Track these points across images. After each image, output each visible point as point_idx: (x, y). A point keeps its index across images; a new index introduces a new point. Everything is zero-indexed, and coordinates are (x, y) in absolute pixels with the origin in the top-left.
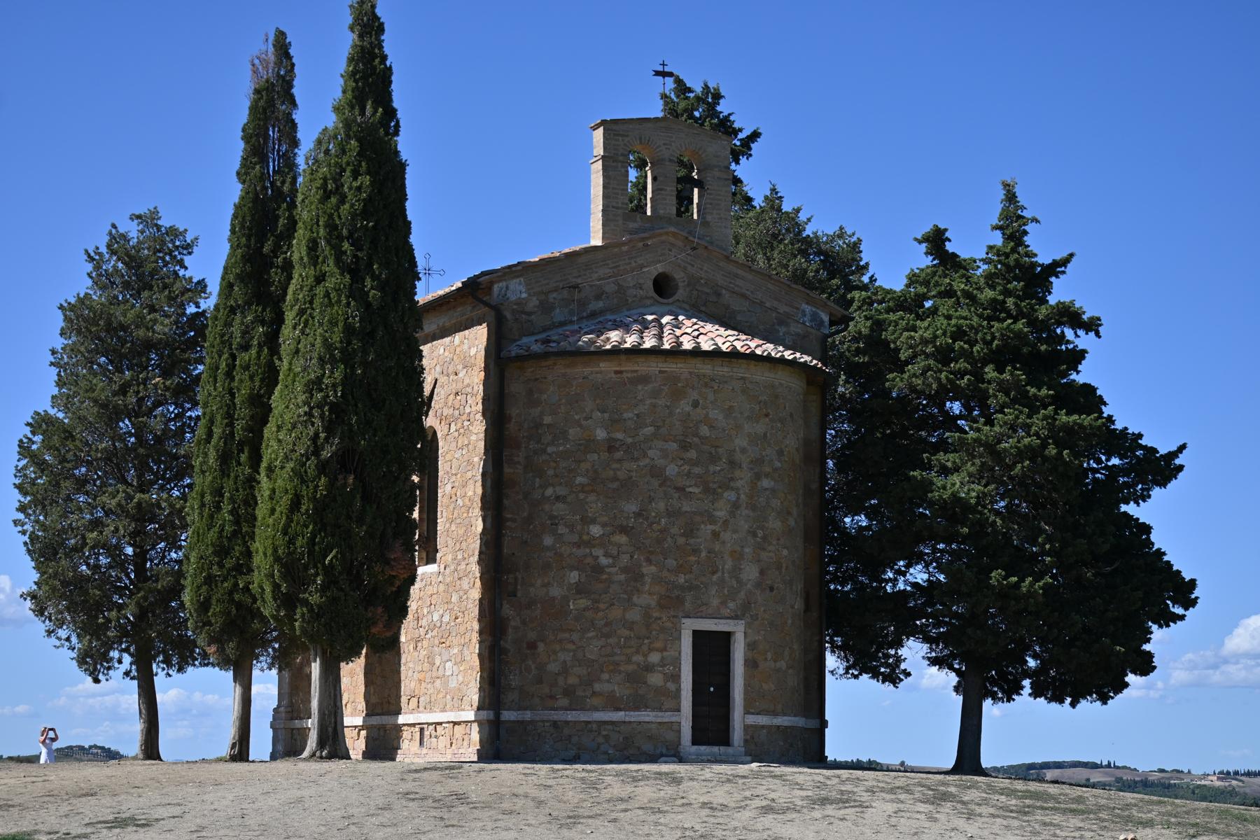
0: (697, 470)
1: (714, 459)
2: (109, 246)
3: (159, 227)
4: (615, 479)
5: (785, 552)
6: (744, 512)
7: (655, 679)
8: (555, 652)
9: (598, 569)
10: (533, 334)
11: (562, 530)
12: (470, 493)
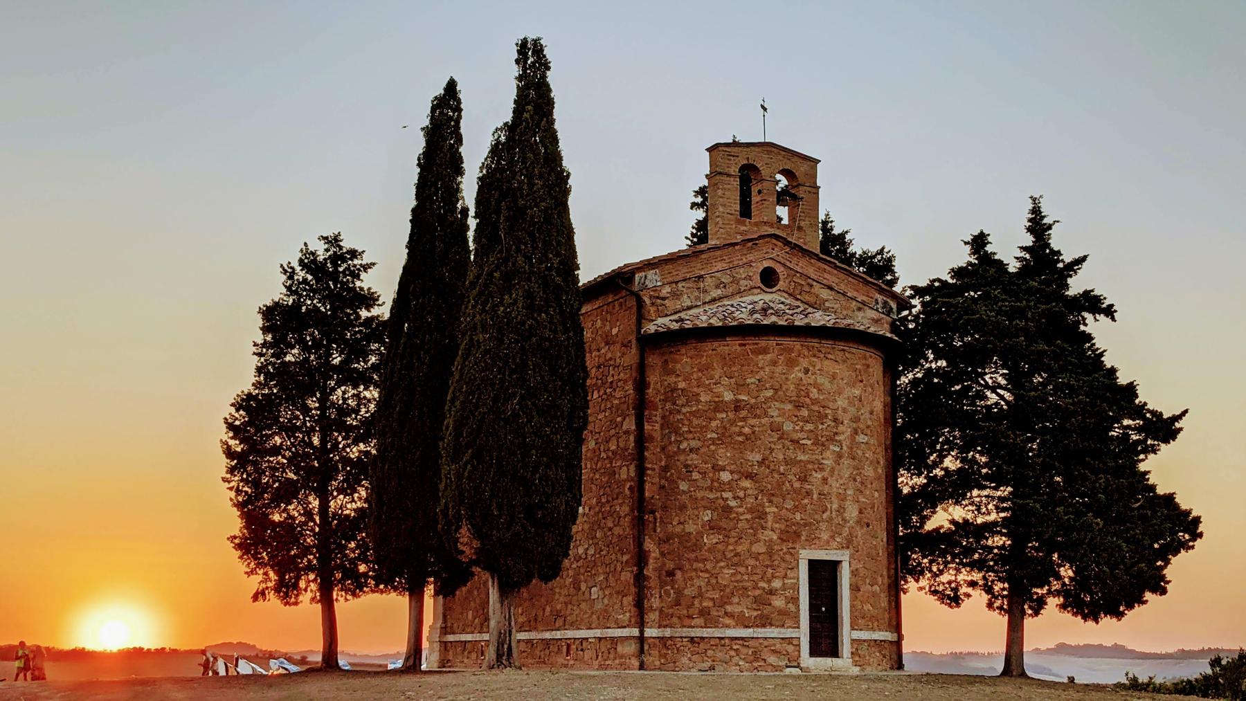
0: (809, 427)
1: (822, 418)
2: (301, 261)
3: (341, 248)
4: (741, 434)
5: (876, 494)
6: (846, 462)
7: (778, 602)
8: (691, 579)
9: (727, 510)
10: (667, 315)
11: (695, 475)
12: (613, 448)
